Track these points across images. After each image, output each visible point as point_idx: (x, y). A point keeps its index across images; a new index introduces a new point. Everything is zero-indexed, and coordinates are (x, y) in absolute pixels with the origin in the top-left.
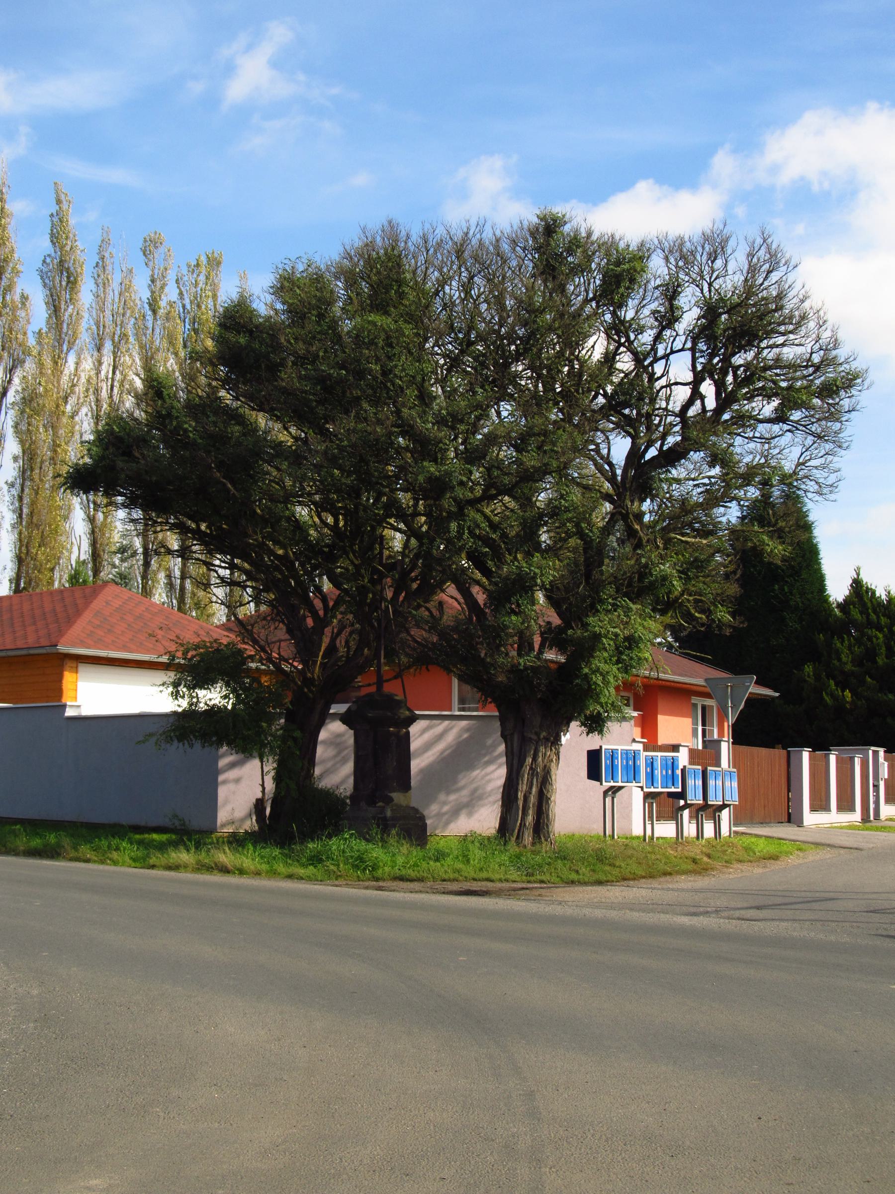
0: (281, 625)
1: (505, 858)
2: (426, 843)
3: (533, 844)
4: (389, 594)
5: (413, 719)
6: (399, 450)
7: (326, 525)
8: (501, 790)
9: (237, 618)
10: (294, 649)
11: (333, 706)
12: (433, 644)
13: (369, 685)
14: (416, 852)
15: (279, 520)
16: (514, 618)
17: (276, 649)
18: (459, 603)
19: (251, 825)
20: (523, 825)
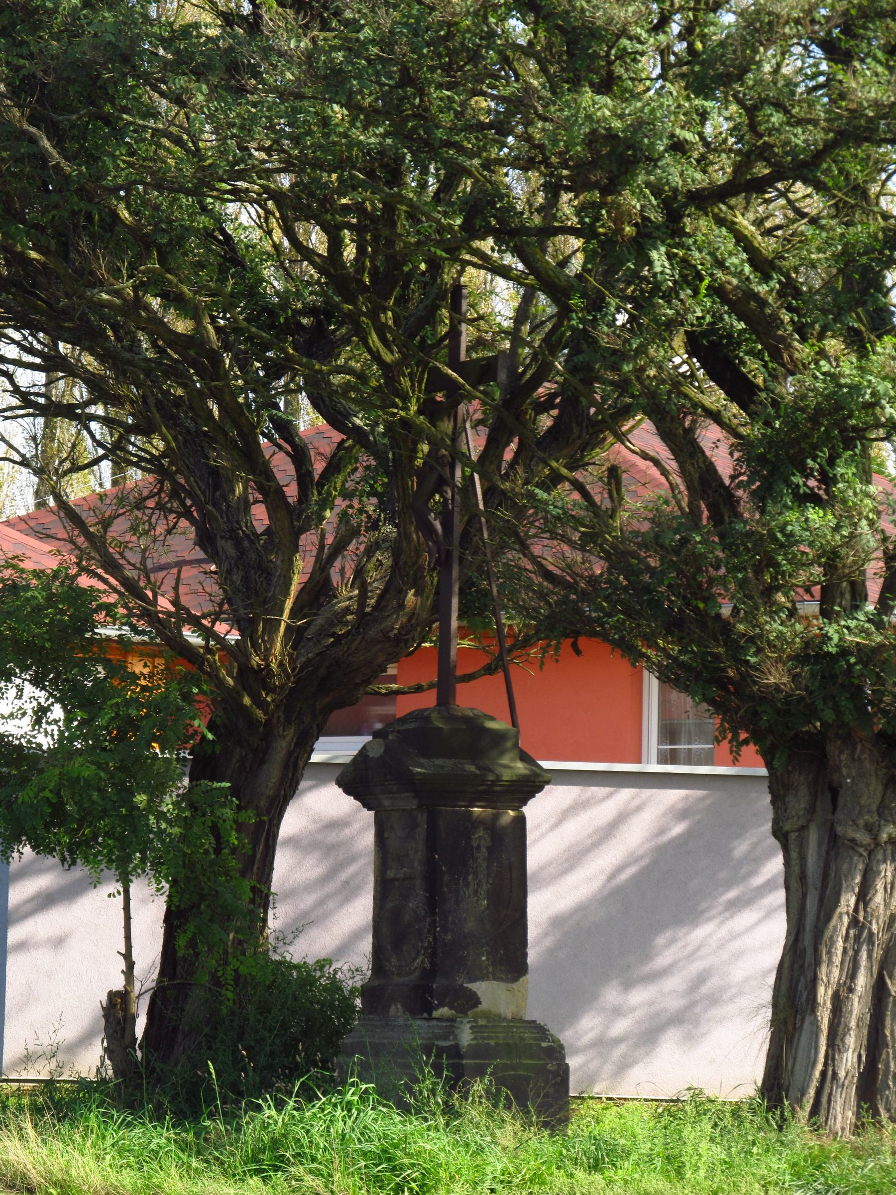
0: (184, 523)
1: (777, 1165)
2: (566, 1120)
3: (858, 1128)
4: (475, 443)
5: (532, 785)
6: (509, 55)
7: (307, 253)
8: (771, 979)
9: (62, 504)
10: (215, 589)
11: (323, 741)
12: (593, 580)
13: (419, 689)
14: (542, 1144)
15: (179, 241)
16: (814, 515)
17: (169, 583)
18: (664, 473)
19: (91, 1062)
20: (829, 1076)
